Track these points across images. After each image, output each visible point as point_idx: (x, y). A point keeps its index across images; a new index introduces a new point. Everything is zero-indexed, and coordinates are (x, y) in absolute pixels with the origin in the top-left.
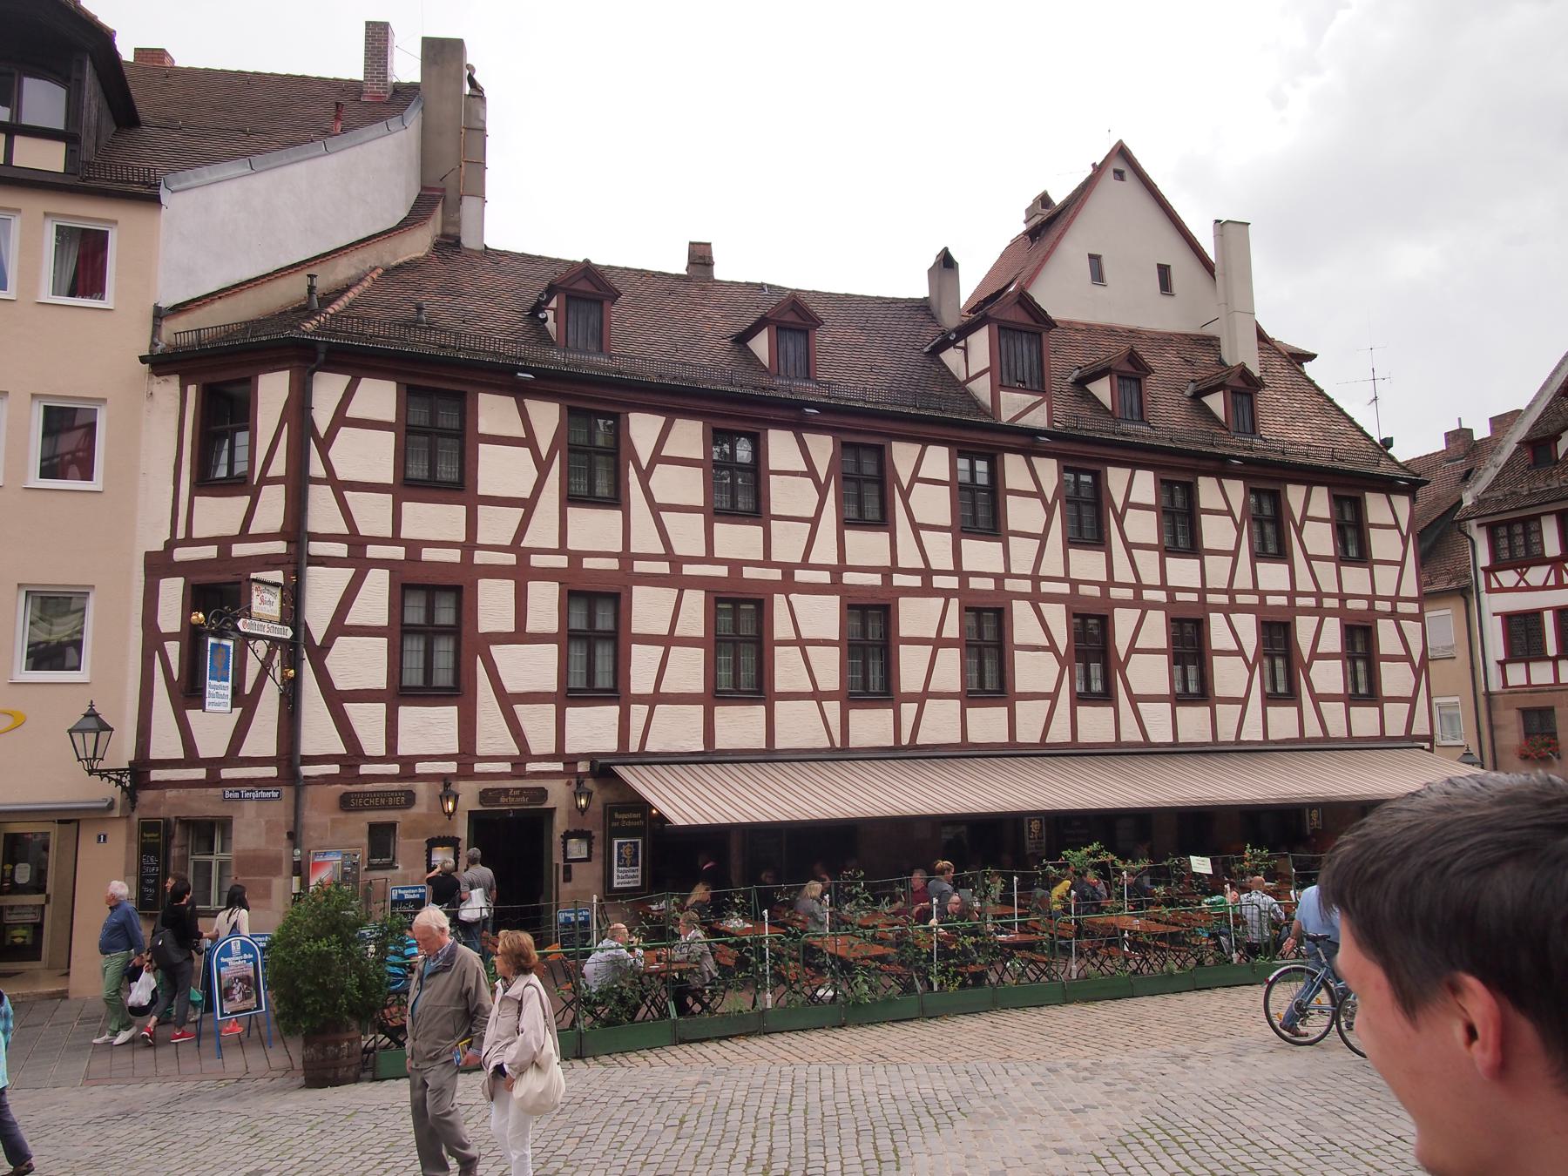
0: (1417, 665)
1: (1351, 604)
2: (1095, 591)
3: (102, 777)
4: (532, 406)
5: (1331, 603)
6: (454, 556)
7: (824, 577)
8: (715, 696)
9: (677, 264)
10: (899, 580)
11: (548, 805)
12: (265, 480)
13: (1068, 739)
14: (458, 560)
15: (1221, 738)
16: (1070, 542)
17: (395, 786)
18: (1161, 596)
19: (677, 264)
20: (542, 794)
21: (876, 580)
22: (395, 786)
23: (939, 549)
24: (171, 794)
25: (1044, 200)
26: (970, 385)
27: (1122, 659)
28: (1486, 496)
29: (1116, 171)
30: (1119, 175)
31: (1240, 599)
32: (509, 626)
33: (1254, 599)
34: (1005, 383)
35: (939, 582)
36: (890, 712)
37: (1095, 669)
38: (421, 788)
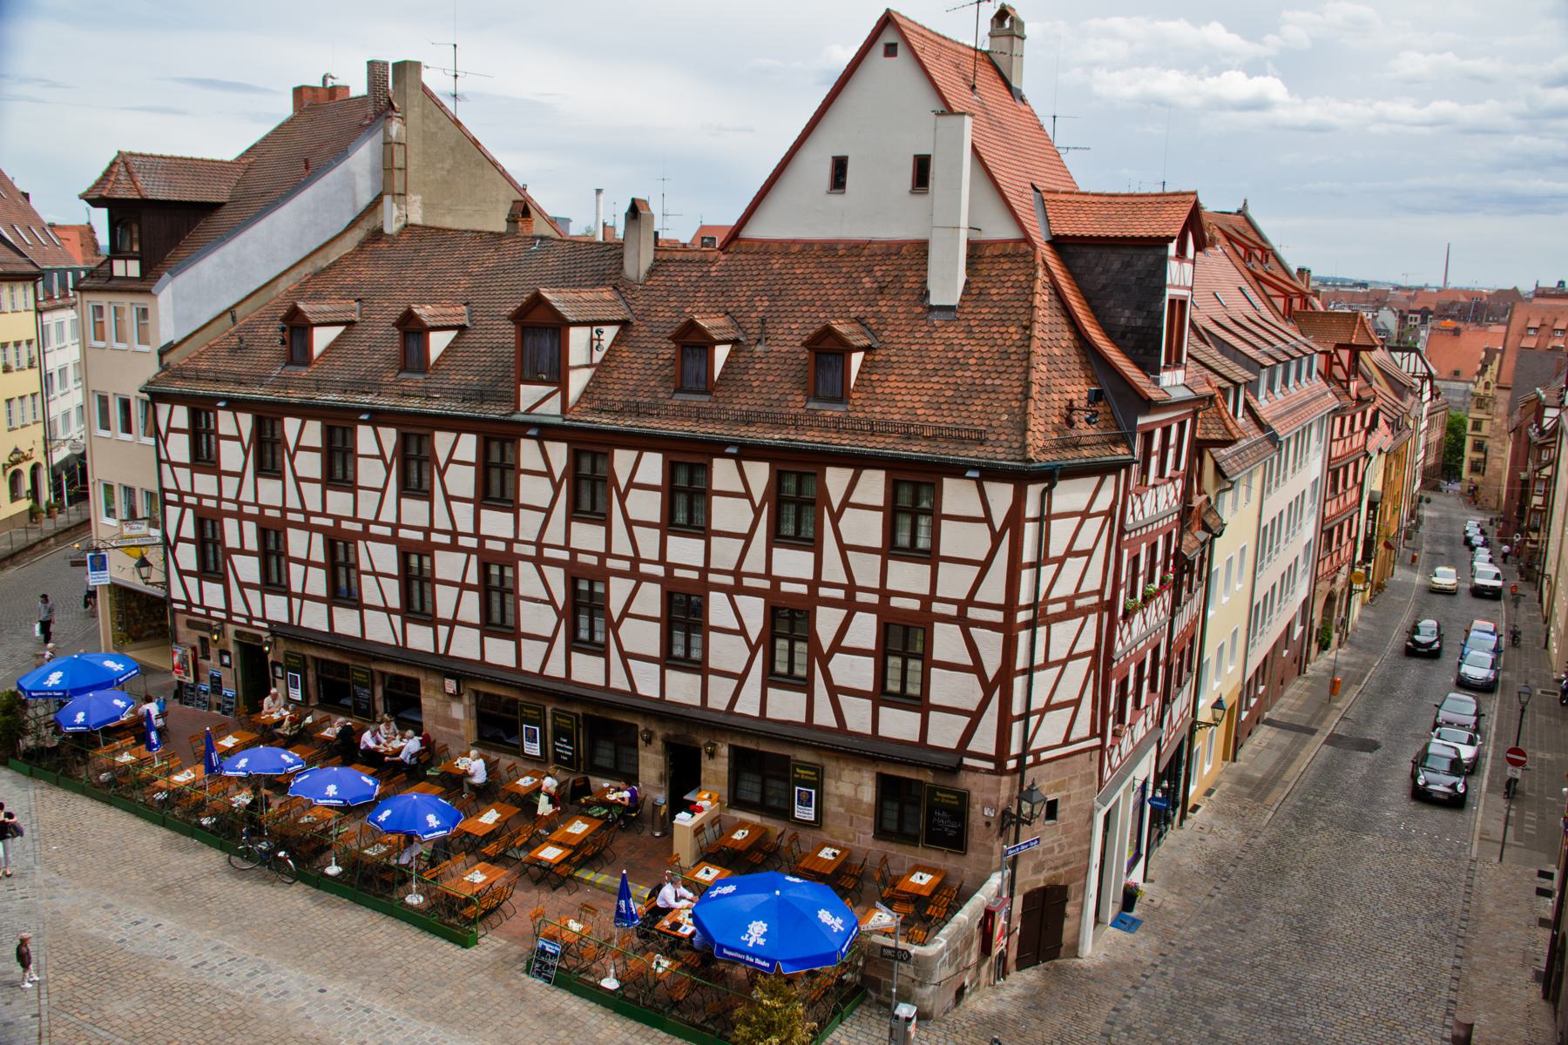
4: (748, 466)
7: (387, 531)
15: (711, 705)
17: (205, 620)
18: (659, 571)
23: (648, 542)
33: (766, 584)
34: (527, 376)
35: (463, 541)
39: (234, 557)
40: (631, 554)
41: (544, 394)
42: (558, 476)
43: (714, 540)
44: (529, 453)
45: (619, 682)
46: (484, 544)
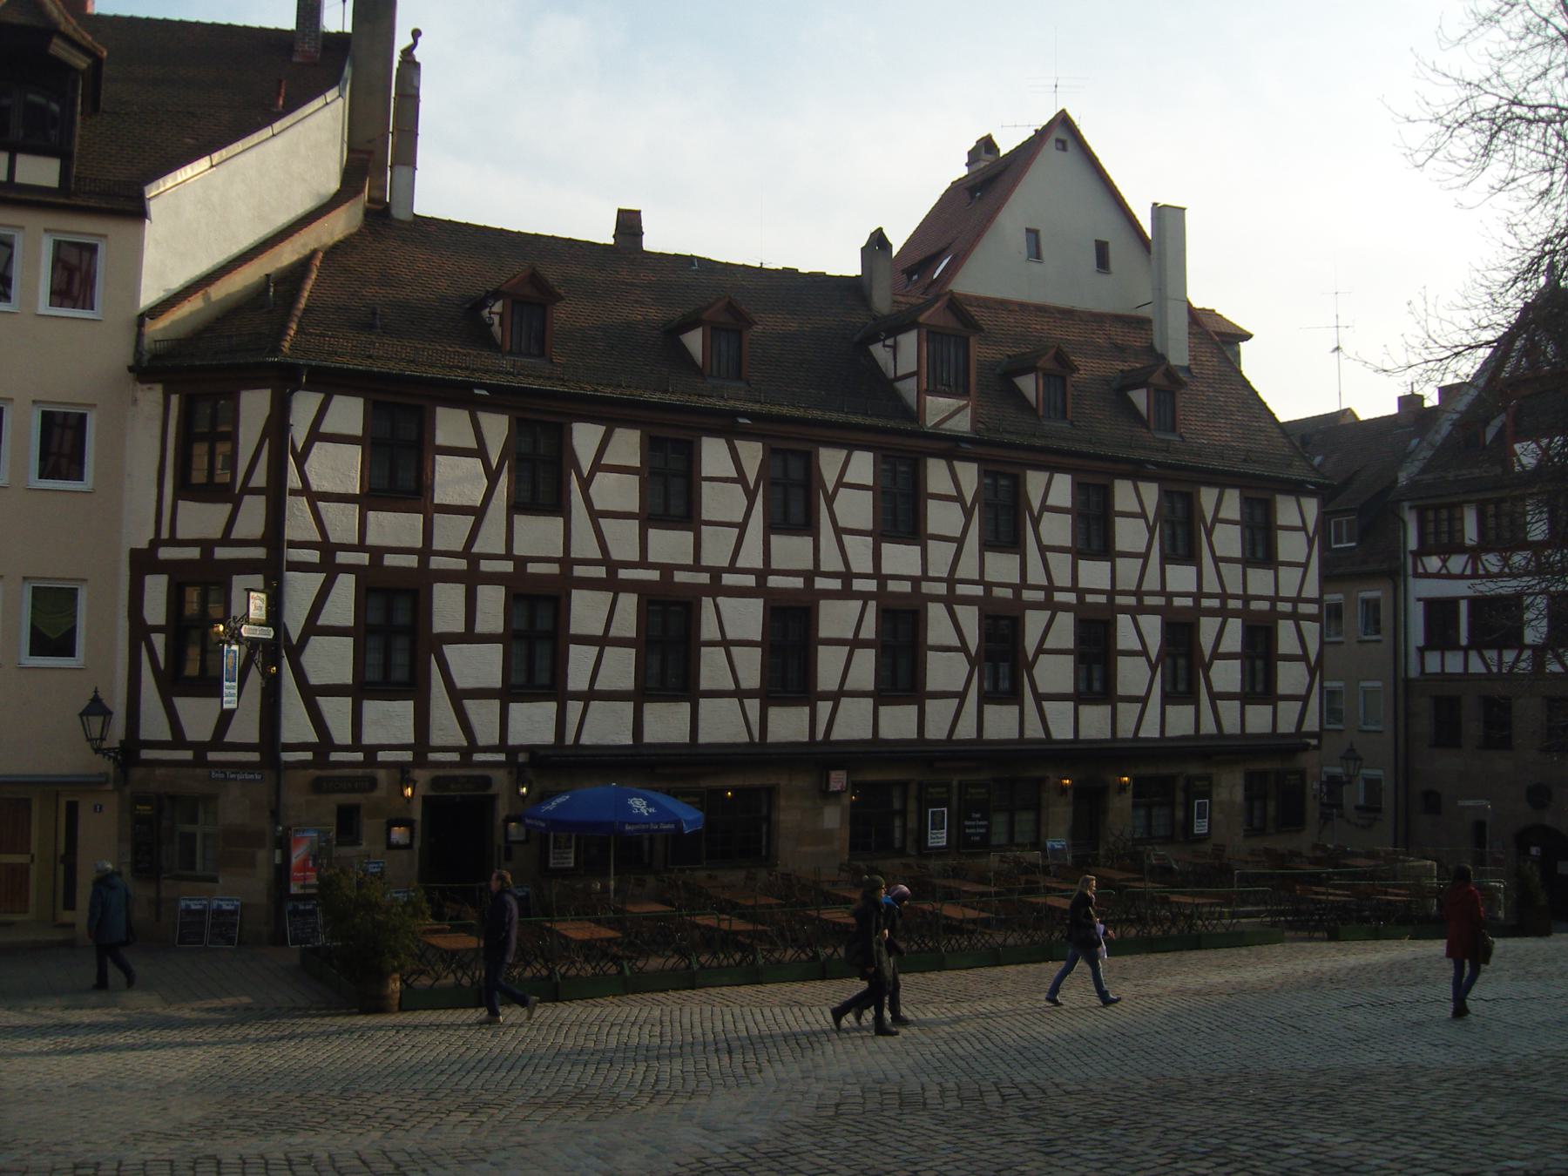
0: (1313, 663)
1: (1255, 605)
2: (1007, 593)
3: (104, 755)
4: (486, 419)
5: (1234, 604)
6: (412, 561)
7: (750, 581)
8: (642, 694)
9: (603, 233)
10: (821, 583)
11: (491, 792)
12: (247, 490)
13: (974, 736)
14: (1163, 603)
15: (1120, 735)
16: (986, 545)
17: (360, 772)
19: (603, 233)
20: (486, 782)
21: (798, 583)
22: (360, 772)
23: (860, 553)
24: (159, 772)
25: (987, 144)
26: (898, 385)
27: (1030, 659)
28: (1417, 478)
29: (1058, 140)
30: (1062, 145)
31: (1148, 601)
32: (460, 627)
35: (858, 585)
36: (807, 710)
37: (1004, 668)
38: (382, 774)
39: (450, 651)
40: (1045, 582)
41: (952, 409)
42: (969, 500)
43: (1119, 561)
44: (937, 476)
45: (1034, 731)
46: (1172, 602)
